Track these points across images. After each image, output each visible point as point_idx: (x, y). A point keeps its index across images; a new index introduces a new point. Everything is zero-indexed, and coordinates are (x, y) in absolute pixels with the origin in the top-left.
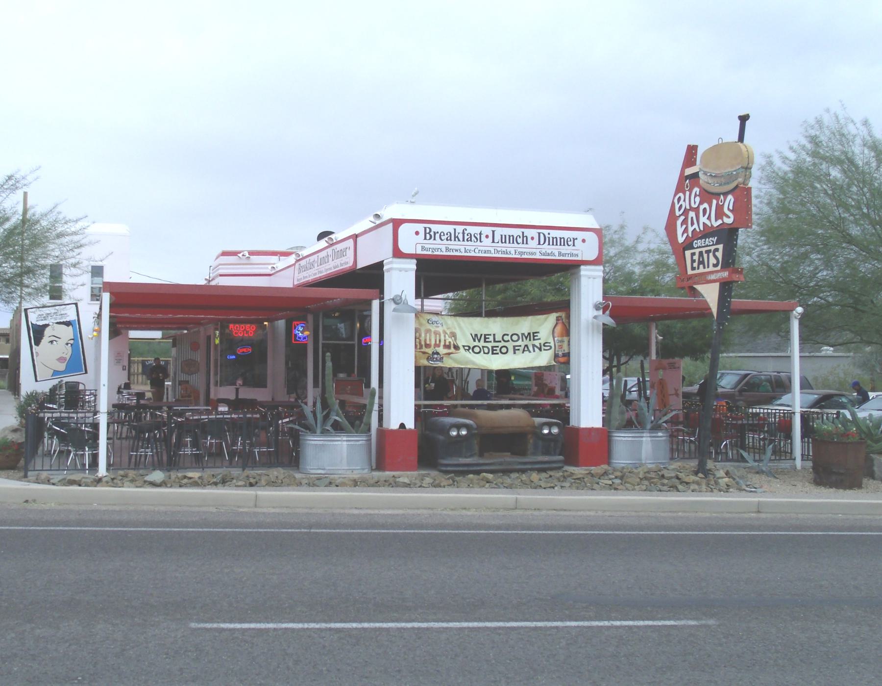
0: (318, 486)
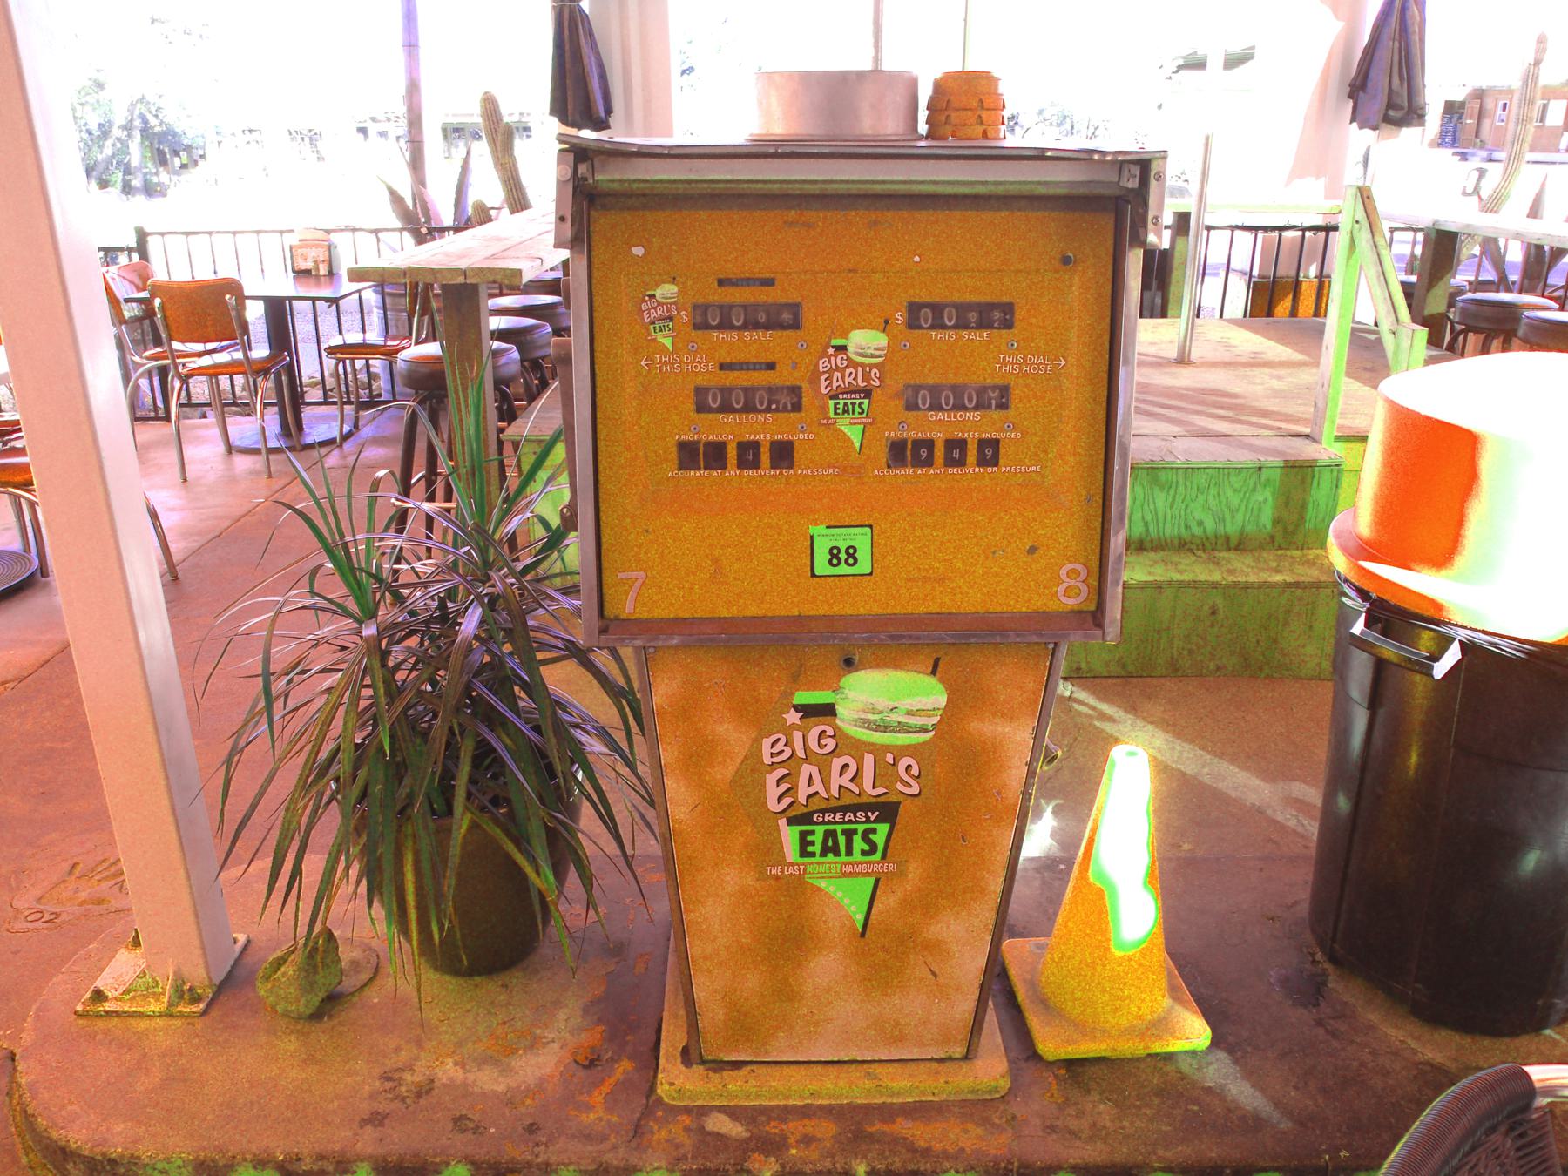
0: (1348, 262)
